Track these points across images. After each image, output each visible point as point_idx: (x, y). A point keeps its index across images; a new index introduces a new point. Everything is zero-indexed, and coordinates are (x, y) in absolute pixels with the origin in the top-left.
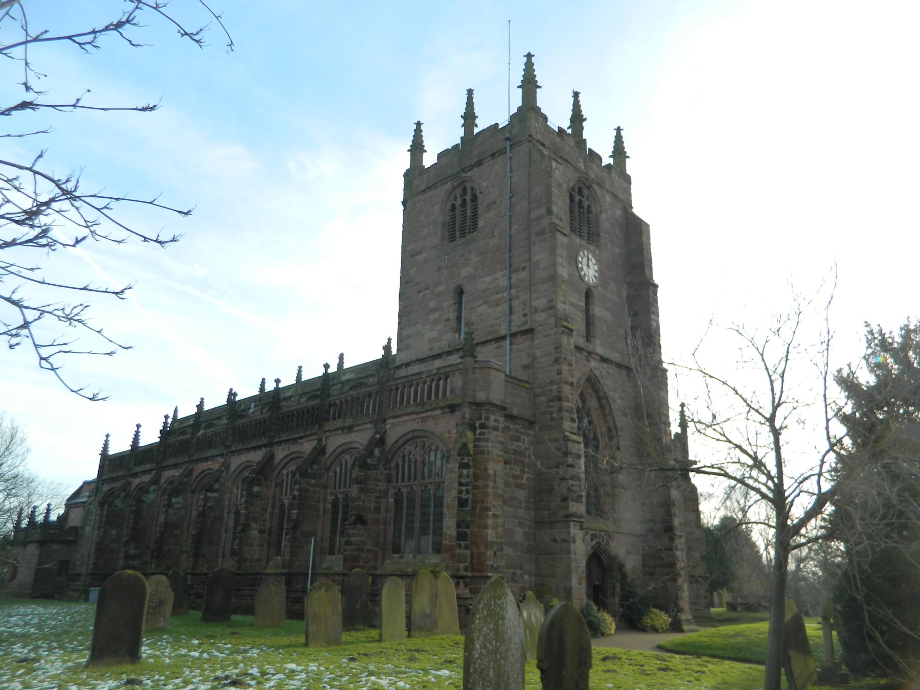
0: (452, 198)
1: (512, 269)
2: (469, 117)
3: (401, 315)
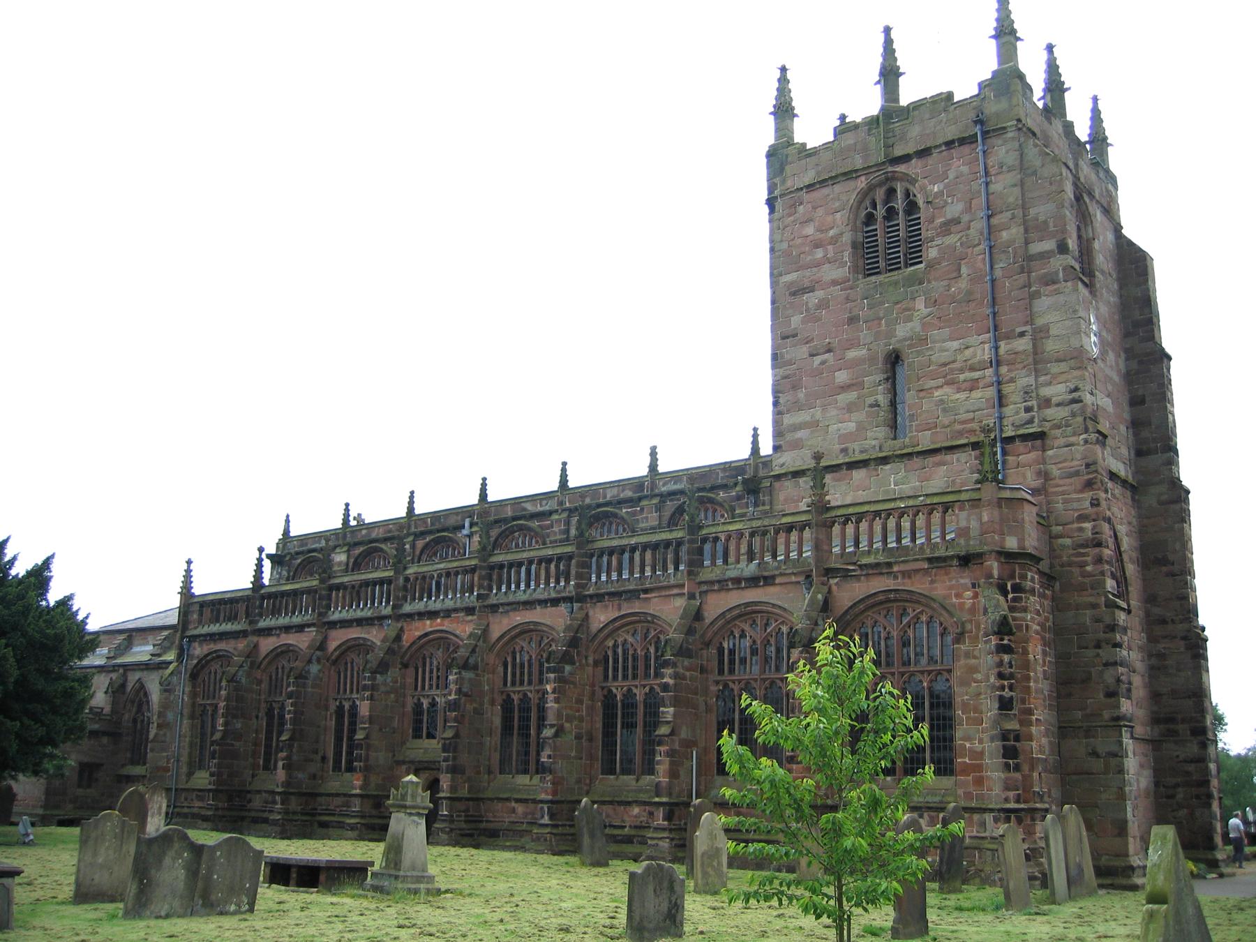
0: (867, 202)
1: (998, 333)
2: (890, 75)
3: (776, 392)
